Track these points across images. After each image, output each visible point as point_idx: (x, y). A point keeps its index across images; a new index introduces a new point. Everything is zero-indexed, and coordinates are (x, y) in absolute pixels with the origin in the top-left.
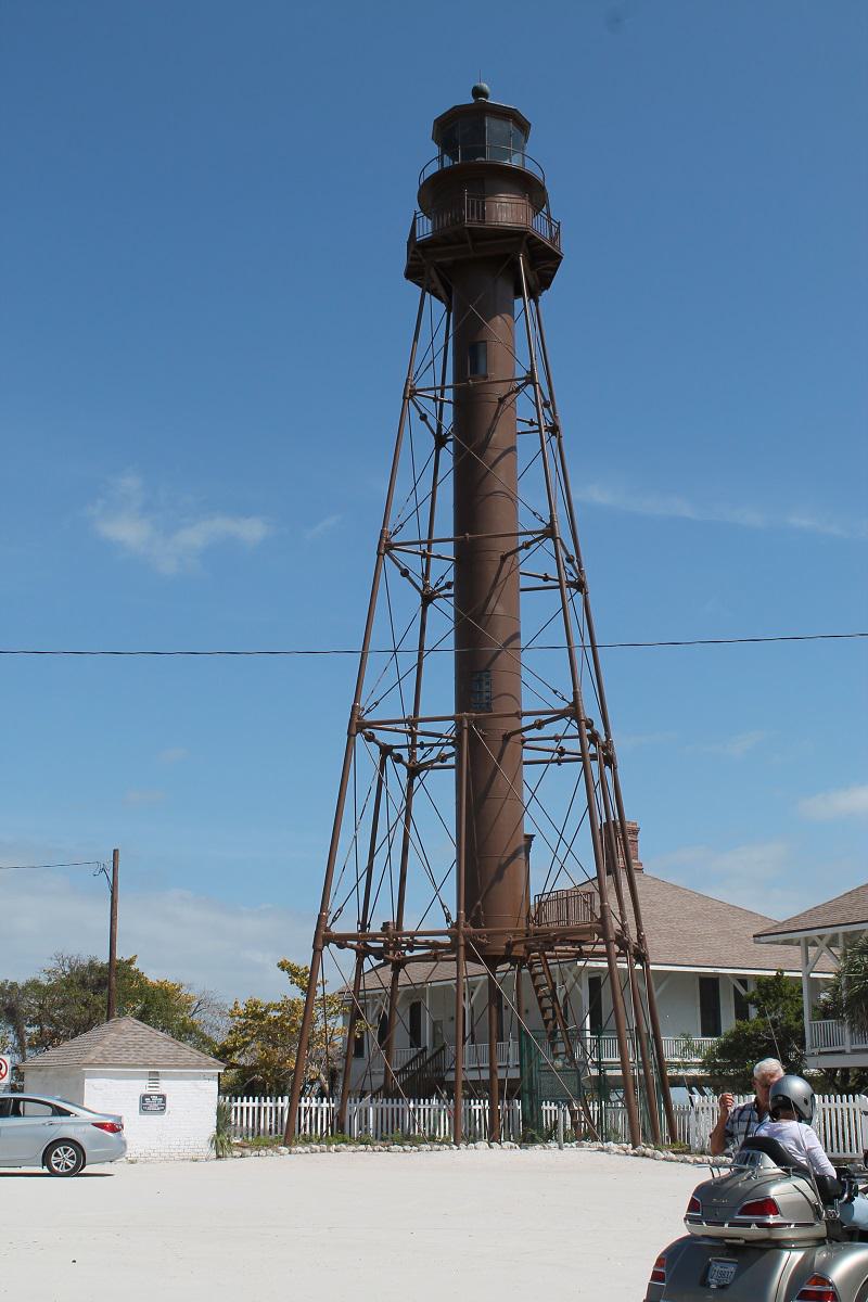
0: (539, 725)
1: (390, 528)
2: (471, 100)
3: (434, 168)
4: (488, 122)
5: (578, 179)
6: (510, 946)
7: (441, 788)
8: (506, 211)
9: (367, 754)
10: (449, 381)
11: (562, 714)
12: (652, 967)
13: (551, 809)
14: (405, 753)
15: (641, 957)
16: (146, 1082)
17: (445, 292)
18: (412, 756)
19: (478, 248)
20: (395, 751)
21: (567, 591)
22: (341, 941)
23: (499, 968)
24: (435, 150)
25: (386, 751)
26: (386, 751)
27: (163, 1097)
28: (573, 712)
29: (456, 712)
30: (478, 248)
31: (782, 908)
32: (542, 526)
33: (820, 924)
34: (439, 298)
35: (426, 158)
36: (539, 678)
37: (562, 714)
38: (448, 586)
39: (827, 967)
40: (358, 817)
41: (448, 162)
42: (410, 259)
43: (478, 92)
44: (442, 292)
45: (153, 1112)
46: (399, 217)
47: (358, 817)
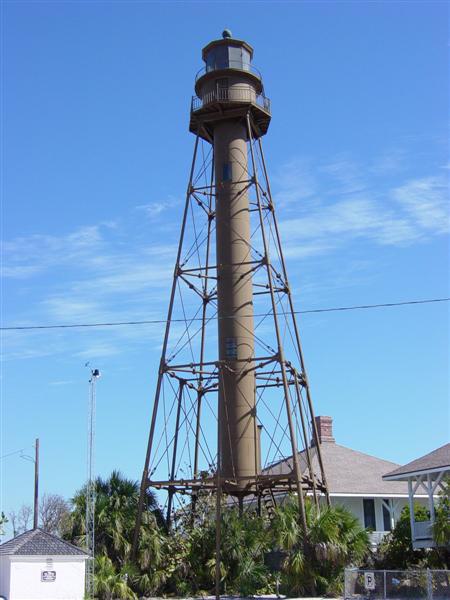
0: (261, 366)
1: (181, 263)
2: (222, 38)
3: (204, 73)
4: (230, 49)
5: (276, 77)
6: (249, 486)
7: (212, 399)
8: (244, 93)
9: (170, 385)
10: (213, 262)
11: (273, 359)
12: (330, 495)
13: (268, 405)
14: (195, 384)
15: (324, 490)
16: (45, 564)
17: (209, 138)
18: (200, 384)
19: (225, 117)
20: (188, 382)
21: (275, 294)
22: (159, 485)
23: (245, 498)
24: (204, 64)
25: (183, 382)
26: (183, 382)
27: (54, 572)
28: (278, 358)
29: (220, 359)
30: (225, 117)
31: (403, 458)
32: (261, 258)
33: (417, 469)
34: (206, 140)
35: (200, 68)
36: (258, 334)
37: (273, 359)
38: (214, 386)
39: (431, 495)
40: (167, 413)
41: (210, 70)
42: (192, 118)
43: (225, 34)
44: (210, 139)
45: (49, 581)
46: (185, 101)
47: (167, 413)
